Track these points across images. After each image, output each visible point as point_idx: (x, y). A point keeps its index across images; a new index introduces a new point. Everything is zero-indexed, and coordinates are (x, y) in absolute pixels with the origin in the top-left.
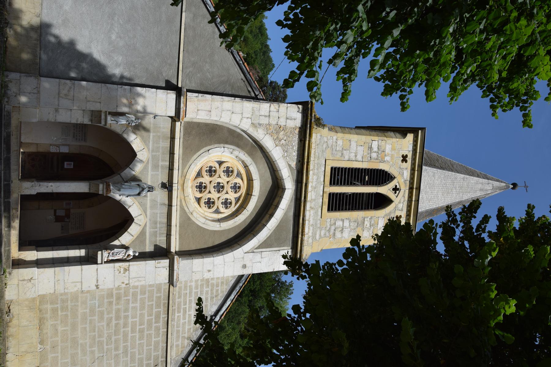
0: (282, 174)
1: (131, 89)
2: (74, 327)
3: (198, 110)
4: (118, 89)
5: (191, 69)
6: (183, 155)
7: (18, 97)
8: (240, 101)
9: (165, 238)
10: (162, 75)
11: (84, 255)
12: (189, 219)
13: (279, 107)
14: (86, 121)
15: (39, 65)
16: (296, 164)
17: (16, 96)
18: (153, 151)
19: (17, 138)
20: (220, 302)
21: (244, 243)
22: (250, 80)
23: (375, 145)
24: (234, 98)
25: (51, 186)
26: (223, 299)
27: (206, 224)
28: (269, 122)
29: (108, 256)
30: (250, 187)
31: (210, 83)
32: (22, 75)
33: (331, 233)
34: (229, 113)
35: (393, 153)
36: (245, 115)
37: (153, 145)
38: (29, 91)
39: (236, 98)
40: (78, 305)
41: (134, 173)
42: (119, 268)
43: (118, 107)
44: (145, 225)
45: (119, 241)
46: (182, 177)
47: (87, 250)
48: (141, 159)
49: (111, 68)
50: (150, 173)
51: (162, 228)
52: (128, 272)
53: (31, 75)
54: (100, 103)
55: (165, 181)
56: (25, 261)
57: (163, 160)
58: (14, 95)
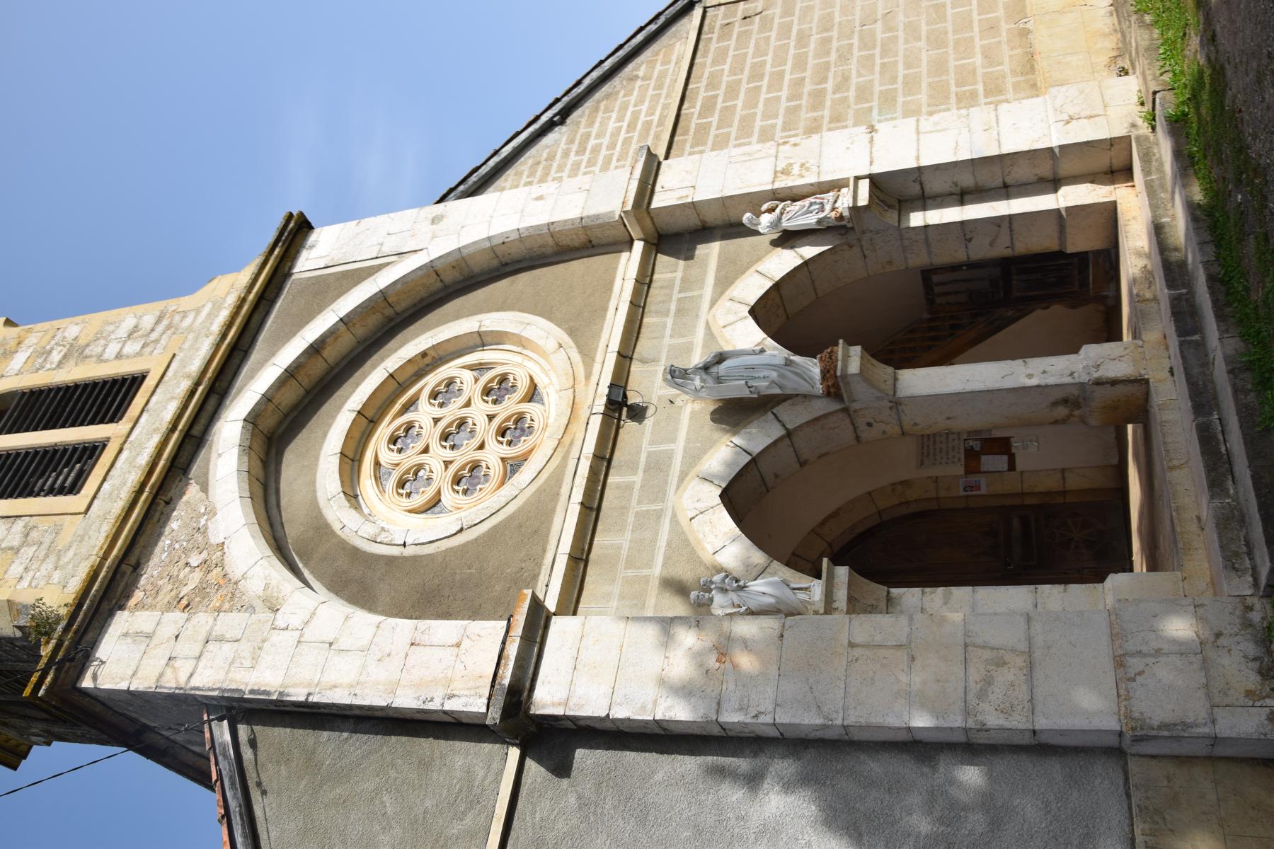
0: (239, 458)
1: (718, 712)
2: (939, 66)
3: (458, 645)
4: (771, 708)
5: (455, 829)
6: (553, 511)
7: (1207, 634)
8: (290, 690)
9: (656, 277)
10: (579, 797)
11: (911, 214)
12: (571, 333)
13: (161, 675)
15: (1130, 808)
16: (182, 494)
17: (1218, 635)
18: (659, 515)
19: (1177, 509)
20: (532, 152)
21: (420, 273)
22: (233, 784)
24: (311, 699)
25: (1030, 376)
26: (523, 159)
27: (522, 323)
28: (215, 620)
29: (835, 202)
30: (359, 442)
31: (393, 773)
32: (1206, 730)
33: (165, 322)
34: (344, 643)
36: (292, 637)
37: (657, 534)
38: (1162, 659)
39: (302, 699)
40: (929, 106)
41: (737, 440)
42: (804, 172)
43: (777, 633)
44: (713, 303)
45: (801, 256)
46: (572, 443)
47: (903, 225)
48: (707, 485)
49: (802, 816)
50: (679, 447)
51: (663, 302)
52: (779, 169)
53: (1166, 733)
54: (852, 645)
55: (629, 427)
56: (1092, 182)
57: (629, 487)
58: (1223, 641)
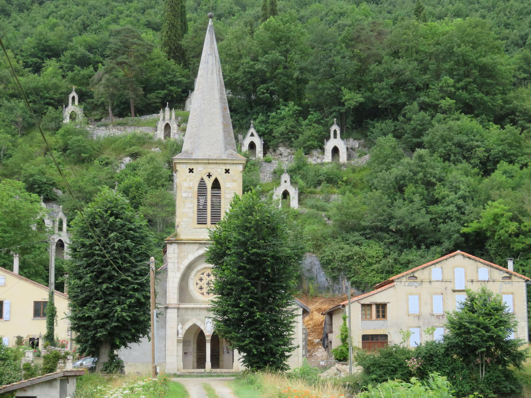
14: (181, 344)
23: (184, 195)
35: (188, 180)
